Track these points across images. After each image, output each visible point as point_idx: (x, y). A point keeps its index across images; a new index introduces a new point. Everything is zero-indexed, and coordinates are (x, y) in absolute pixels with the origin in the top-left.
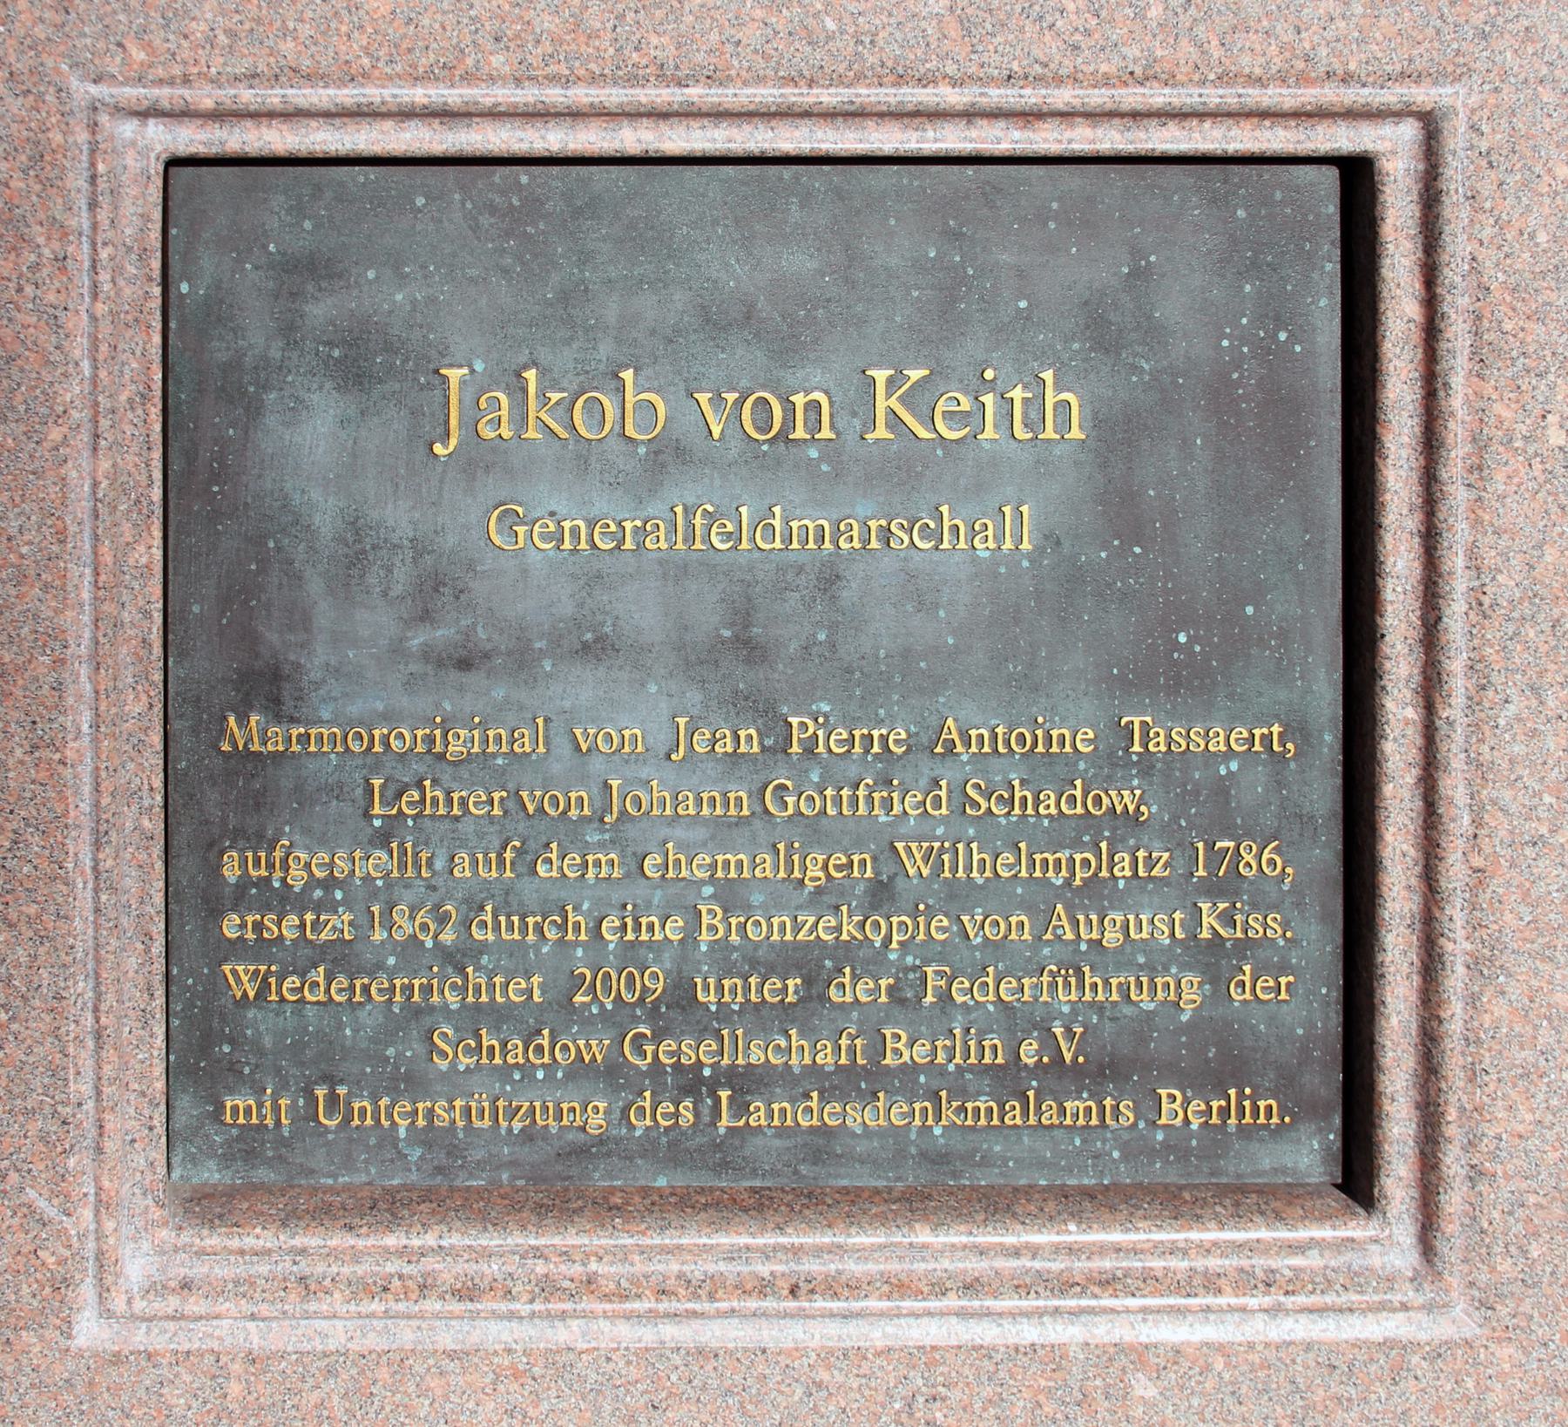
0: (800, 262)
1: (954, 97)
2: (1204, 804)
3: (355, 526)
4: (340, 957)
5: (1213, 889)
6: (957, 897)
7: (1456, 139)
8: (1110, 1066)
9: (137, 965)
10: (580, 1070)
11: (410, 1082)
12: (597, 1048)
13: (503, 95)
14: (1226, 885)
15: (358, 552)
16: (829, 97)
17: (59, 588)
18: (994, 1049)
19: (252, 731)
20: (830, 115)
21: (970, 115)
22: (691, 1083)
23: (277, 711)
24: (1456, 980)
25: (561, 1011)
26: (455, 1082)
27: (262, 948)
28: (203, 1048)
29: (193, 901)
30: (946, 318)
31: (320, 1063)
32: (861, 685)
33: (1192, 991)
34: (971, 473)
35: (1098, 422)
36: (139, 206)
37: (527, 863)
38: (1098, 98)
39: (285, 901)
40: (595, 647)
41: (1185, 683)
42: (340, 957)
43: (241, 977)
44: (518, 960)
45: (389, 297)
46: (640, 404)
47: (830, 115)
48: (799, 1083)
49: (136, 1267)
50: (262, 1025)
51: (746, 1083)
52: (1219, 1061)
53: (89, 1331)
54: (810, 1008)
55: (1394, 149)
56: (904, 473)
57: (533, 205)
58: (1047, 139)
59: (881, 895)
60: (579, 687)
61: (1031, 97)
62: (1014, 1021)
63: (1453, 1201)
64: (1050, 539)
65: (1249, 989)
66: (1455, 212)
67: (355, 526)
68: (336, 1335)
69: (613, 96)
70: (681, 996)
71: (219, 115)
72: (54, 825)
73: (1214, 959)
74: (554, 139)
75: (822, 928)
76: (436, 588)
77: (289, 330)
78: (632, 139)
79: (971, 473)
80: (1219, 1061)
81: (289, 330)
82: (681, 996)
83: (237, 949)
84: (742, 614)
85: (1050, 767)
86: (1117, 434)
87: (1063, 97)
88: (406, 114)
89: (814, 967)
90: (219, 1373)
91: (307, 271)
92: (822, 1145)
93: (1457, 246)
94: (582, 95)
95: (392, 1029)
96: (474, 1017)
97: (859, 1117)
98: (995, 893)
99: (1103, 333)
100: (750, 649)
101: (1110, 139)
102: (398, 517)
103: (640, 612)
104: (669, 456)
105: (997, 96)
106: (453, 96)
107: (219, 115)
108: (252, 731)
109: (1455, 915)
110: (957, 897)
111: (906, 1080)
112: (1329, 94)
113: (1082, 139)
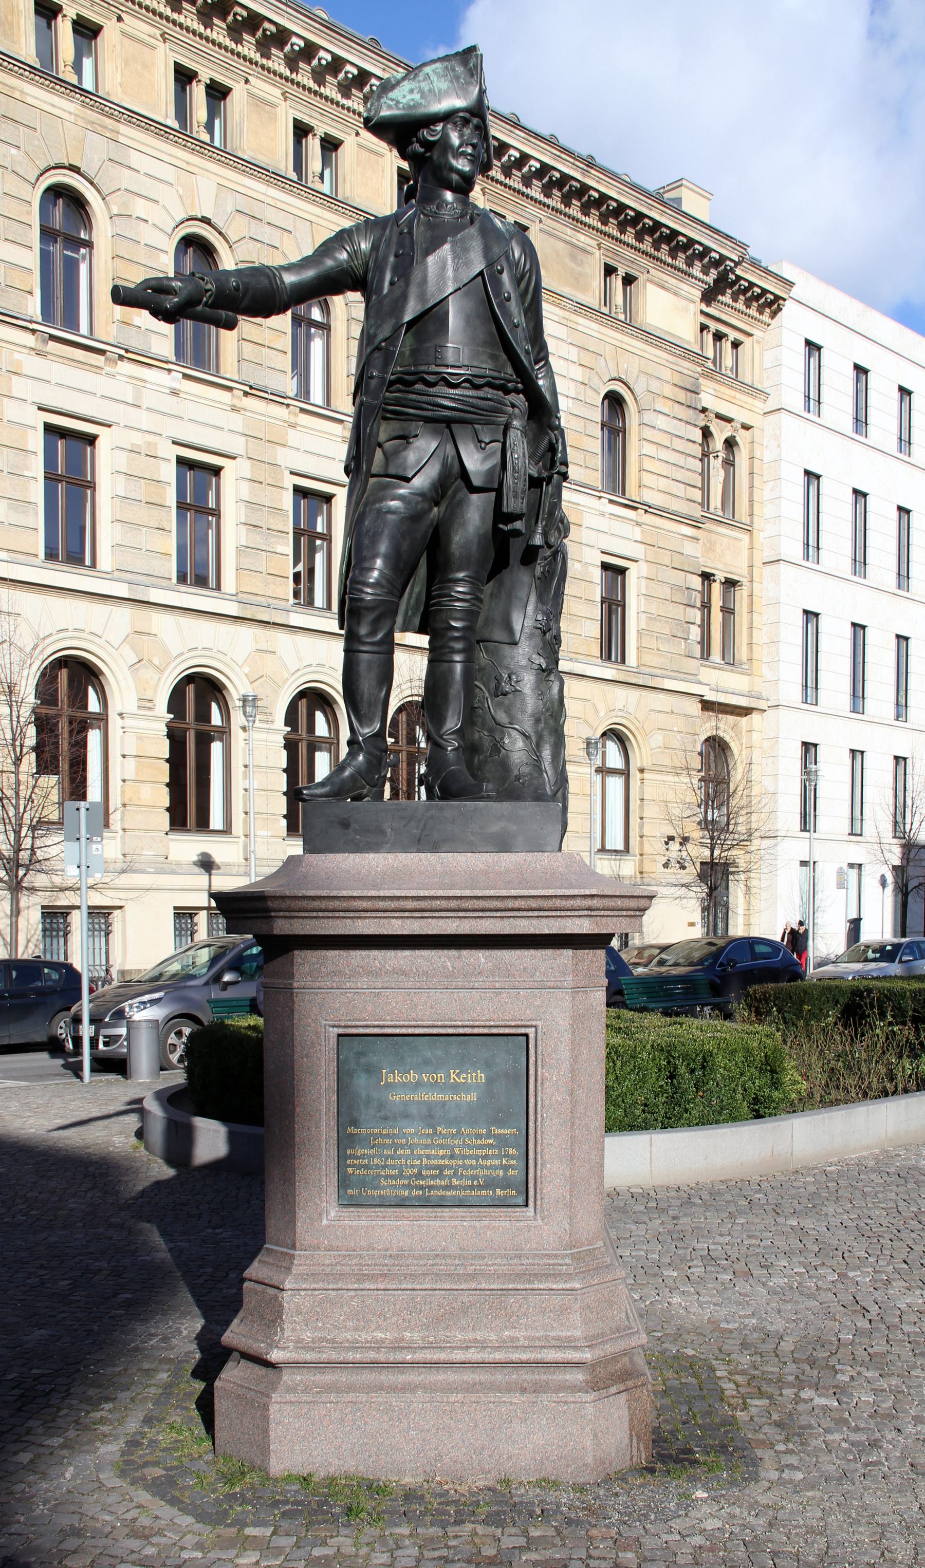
0: (439, 1053)
1: (459, 1023)
2: (503, 1142)
3: (368, 1096)
4: (366, 1167)
5: (505, 1156)
6: (464, 1157)
7: (539, 1030)
8: (490, 1184)
9: (333, 1164)
10: (404, 1185)
11: (377, 1188)
12: (406, 1182)
13: (389, 1023)
14: (507, 1156)
15: (369, 1100)
16: (440, 1023)
17: (320, 1103)
18: (470, 1183)
19: (351, 1130)
20: (441, 1027)
21: (463, 1027)
22: (421, 1188)
23: (356, 1127)
24: (539, 1166)
25: (401, 1176)
26: (384, 1188)
27: (353, 1165)
28: (344, 1182)
29: (342, 1158)
30: (462, 1063)
31: (363, 1183)
32: (449, 1123)
33: (501, 1173)
34: (466, 1088)
35: (486, 1079)
36: (333, 1041)
37: (395, 1151)
38: (483, 1023)
39: (357, 1158)
40: (406, 1116)
41: (501, 1123)
42: (366, 1167)
43: (350, 1170)
44: (393, 1167)
45: (373, 1059)
46: (412, 1076)
47: (441, 1027)
48: (438, 1188)
49: (333, 1214)
50: (353, 1178)
51: (431, 1188)
52: (506, 1184)
53: (325, 1222)
54: (440, 1176)
55: (531, 1032)
56: (456, 1088)
57: (397, 1044)
58: (476, 1031)
59: (452, 1157)
60: (404, 1122)
61: (472, 1023)
62: (473, 1178)
63: (538, 1203)
64: (479, 1099)
65: (511, 1172)
66: (539, 1043)
67: (368, 1096)
68: (363, 1223)
69: (406, 1023)
70: (420, 1173)
71: (345, 1027)
72: (319, 1141)
73: (505, 1168)
74: (398, 1031)
75: (441, 1162)
76: (381, 1106)
77: (358, 1064)
78: (410, 1031)
79: (466, 1088)
80: (506, 1184)
81: (358, 1064)
82: (420, 1173)
83: (350, 1166)
84: (430, 1110)
85: (479, 1136)
86: (490, 1081)
87: (477, 1023)
88: (374, 1026)
89: (441, 1168)
90: (345, 1229)
91: (362, 1054)
92: (443, 1197)
93: (540, 1048)
94: (401, 1023)
95: (374, 1179)
96: (387, 1177)
97: (448, 1193)
98: (470, 1157)
99: (488, 1065)
100: (431, 1116)
101: (486, 1031)
102: (375, 1095)
103: (414, 1110)
104: (418, 1084)
105: (466, 1023)
106: (381, 1023)
107: (345, 1027)
108: (351, 1130)
109: (539, 1156)
110: (464, 1157)
111: (456, 1188)
112: (519, 1023)
113: (481, 1031)
